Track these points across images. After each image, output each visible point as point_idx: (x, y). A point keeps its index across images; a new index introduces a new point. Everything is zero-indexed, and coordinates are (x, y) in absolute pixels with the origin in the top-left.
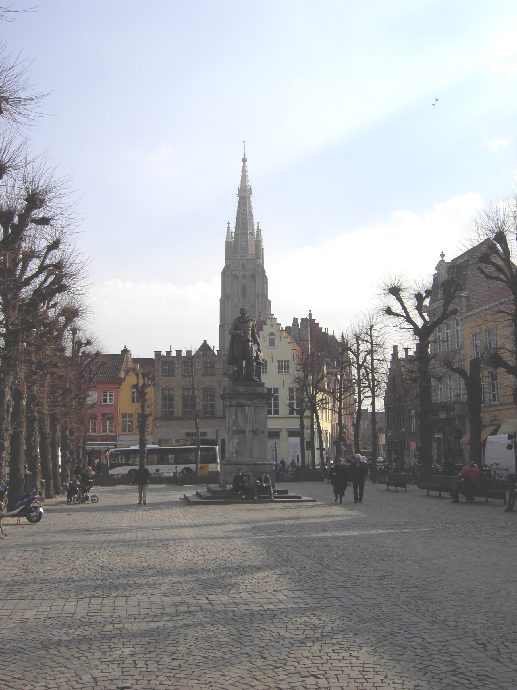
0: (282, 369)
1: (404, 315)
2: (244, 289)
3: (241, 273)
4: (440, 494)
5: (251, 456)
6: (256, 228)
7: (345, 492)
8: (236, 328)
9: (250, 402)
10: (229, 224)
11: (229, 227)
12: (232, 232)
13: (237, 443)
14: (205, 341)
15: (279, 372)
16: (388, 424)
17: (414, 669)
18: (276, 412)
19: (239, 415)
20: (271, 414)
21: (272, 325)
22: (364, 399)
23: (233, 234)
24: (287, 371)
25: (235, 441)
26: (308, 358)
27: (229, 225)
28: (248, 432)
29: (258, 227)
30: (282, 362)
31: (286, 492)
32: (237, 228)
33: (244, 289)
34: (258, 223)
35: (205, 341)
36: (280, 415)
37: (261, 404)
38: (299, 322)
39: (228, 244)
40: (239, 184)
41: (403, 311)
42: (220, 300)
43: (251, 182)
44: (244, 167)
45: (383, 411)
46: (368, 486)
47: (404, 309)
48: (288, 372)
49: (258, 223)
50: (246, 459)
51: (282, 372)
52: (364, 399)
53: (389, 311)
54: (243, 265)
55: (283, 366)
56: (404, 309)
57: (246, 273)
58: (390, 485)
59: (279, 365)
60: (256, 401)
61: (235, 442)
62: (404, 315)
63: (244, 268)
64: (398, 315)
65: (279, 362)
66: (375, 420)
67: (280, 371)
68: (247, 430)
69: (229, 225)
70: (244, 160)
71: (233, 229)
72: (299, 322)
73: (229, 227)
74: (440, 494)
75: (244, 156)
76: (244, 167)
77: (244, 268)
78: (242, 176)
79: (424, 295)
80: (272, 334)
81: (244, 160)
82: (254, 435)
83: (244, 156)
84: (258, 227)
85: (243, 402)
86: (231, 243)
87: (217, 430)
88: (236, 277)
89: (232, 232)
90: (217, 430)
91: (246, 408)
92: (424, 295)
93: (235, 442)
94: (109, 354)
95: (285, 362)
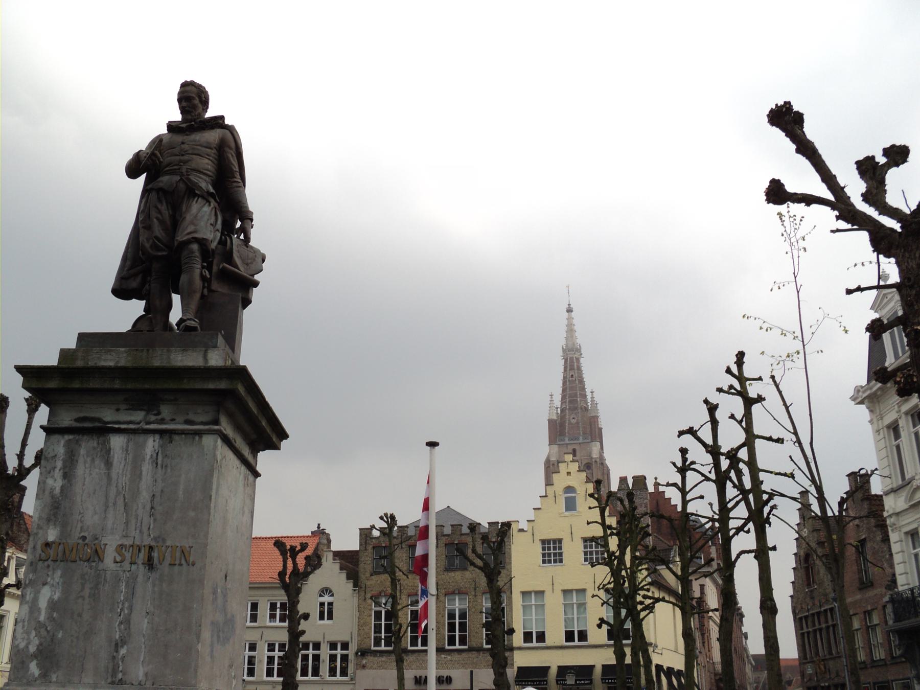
0: (591, 553)
1: (831, 197)
6: (589, 400)
9: (139, 416)
13: (53, 605)
14: (192, 97)
15: (544, 562)
16: (805, 655)
19: (81, 470)
20: (574, 641)
21: (569, 473)
22: (738, 556)
24: (558, 558)
28: (110, 555)
29: (592, 398)
30: (549, 541)
38: (630, 482)
39: (551, 422)
40: (564, 342)
41: (824, 186)
43: (581, 339)
44: (570, 319)
45: (796, 656)
47: (828, 178)
51: (550, 562)
52: (738, 556)
53: (777, 193)
56: (828, 178)
59: (543, 549)
60: (166, 411)
61: (43, 603)
62: (831, 197)
64: (809, 200)
66: (772, 600)
68: (111, 543)
71: (557, 402)
72: (630, 482)
76: (570, 319)
80: (569, 489)
81: (569, 310)
82: (141, 570)
84: (592, 398)
85: (108, 415)
86: (555, 421)
87: (472, 672)
90: (472, 672)
91: (117, 442)
93: (43, 603)
95: (555, 541)
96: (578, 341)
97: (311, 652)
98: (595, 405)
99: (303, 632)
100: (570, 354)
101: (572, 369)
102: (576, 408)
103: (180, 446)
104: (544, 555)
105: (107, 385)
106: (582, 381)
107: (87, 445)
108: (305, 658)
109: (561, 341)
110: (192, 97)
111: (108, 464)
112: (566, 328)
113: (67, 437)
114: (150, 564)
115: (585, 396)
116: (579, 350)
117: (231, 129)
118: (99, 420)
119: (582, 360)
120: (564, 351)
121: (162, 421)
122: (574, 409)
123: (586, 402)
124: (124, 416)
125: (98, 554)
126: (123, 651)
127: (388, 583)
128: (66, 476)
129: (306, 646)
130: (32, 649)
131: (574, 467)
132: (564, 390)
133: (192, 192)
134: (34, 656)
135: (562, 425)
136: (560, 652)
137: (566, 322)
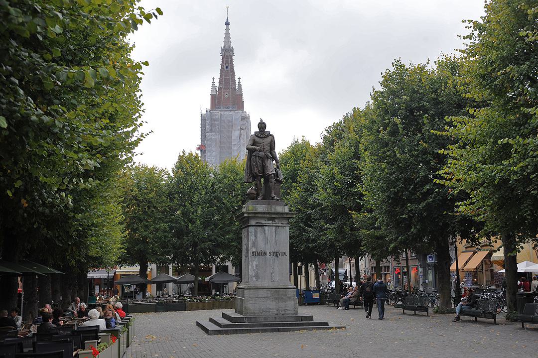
4: (476, 319)
6: (237, 83)
7: (153, 313)
8: (254, 143)
9: (270, 222)
10: (213, 79)
11: (213, 82)
12: (216, 87)
13: (257, 266)
14: (261, 120)
19: (259, 235)
23: (217, 89)
25: (254, 263)
26: (182, 248)
27: (213, 81)
28: (268, 254)
29: (239, 82)
31: (311, 318)
32: (220, 83)
34: (239, 79)
35: (261, 120)
37: (282, 224)
39: (212, 95)
40: (223, 45)
44: (227, 29)
46: (389, 309)
49: (239, 79)
58: (407, 309)
61: (254, 265)
69: (213, 81)
70: (227, 24)
73: (213, 82)
74: (476, 319)
75: (227, 20)
76: (227, 29)
81: (227, 24)
83: (227, 20)
84: (239, 82)
85: (263, 222)
86: (215, 95)
89: (216, 87)
91: (266, 228)
93: (254, 265)
98: (240, 86)
100: (227, 53)
101: (227, 62)
103: (280, 229)
105: (262, 216)
106: (233, 72)
107: (259, 229)
111: (265, 234)
113: (254, 227)
114: (277, 256)
117: (272, 136)
118: (261, 223)
121: (276, 223)
122: (226, 88)
124: (267, 222)
126: (273, 275)
127: (524, 325)
128: (255, 236)
130: (253, 275)
132: (221, 76)
133: (268, 158)
134: (254, 276)
135: (219, 98)
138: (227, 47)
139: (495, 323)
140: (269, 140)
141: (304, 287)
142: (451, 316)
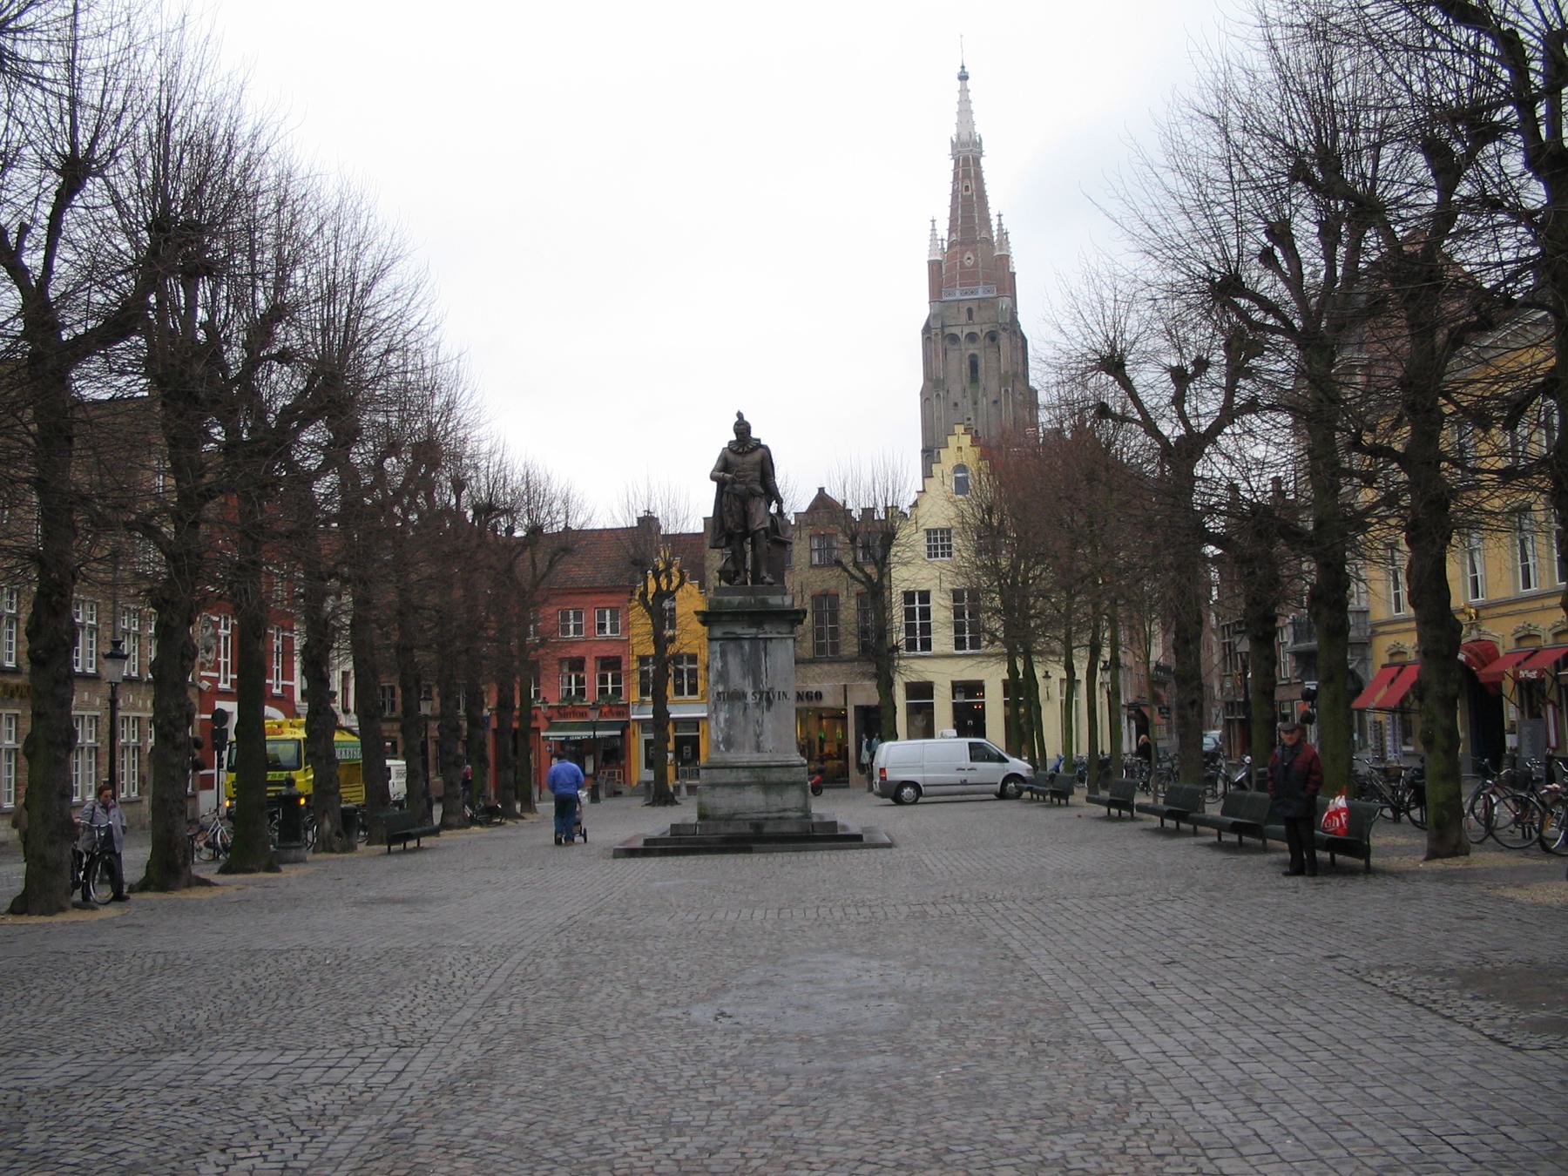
1: (1138, 417)
2: (974, 366)
3: (967, 330)
5: (758, 748)
9: (754, 631)
13: (726, 720)
15: (930, 556)
17: (824, 1166)
18: (927, 645)
19: (730, 658)
25: (722, 716)
29: (1000, 225)
30: (935, 531)
33: (974, 366)
36: (936, 648)
39: (934, 267)
40: (952, 132)
42: (922, 393)
43: (983, 128)
44: (964, 91)
48: (950, 555)
50: (747, 756)
51: (936, 555)
54: (970, 311)
55: (939, 542)
57: (976, 329)
59: (929, 540)
63: (970, 318)
65: (928, 531)
67: (932, 552)
70: (963, 77)
71: (943, 231)
73: (934, 230)
74: (1332, 857)
76: (964, 91)
77: (970, 318)
78: (960, 113)
79: (1190, 370)
81: (963, 77)
84: (1000, 225)
86: (939, 263)
88: (954, 338)
92: (1190, 370)
94: (685, 531)
96: (978, 129)
97: (685, 666)
98: (1004, 234)
99: (672, 639)
102: (974, 242)
104: (929, 548)
107: (732, 645)
108: (679, 674)
109: (949, 130)
110: (742, 428)
112: (956, 108)
115: (987, 221)
116: (978, 144)
117: (766, 448)
119: (983, 161)
120: (954, 145)
123: (990, 231)
125: (744, 696)
129: (678, 658)
131: (967, 440)
133: (753, 494)
136: (953, 661)
137: (957, 97)
138: (965, 137)
139: (1368, 870)
140: (757, 456)
141: (1084, 751)
142: (343, 860)
